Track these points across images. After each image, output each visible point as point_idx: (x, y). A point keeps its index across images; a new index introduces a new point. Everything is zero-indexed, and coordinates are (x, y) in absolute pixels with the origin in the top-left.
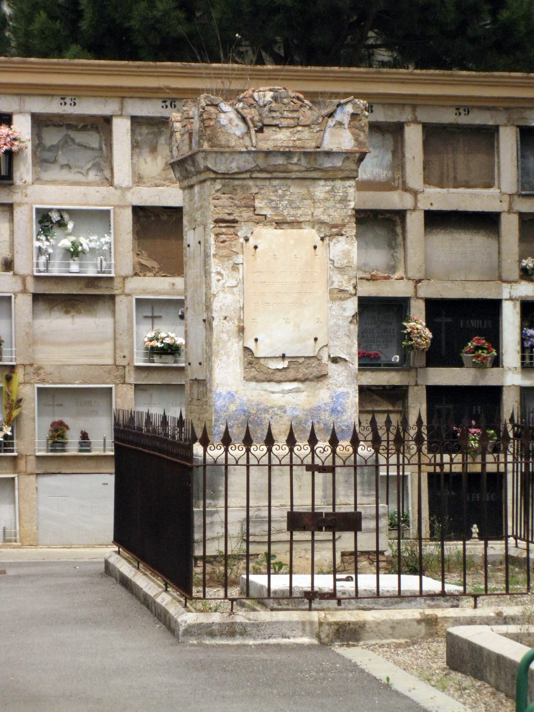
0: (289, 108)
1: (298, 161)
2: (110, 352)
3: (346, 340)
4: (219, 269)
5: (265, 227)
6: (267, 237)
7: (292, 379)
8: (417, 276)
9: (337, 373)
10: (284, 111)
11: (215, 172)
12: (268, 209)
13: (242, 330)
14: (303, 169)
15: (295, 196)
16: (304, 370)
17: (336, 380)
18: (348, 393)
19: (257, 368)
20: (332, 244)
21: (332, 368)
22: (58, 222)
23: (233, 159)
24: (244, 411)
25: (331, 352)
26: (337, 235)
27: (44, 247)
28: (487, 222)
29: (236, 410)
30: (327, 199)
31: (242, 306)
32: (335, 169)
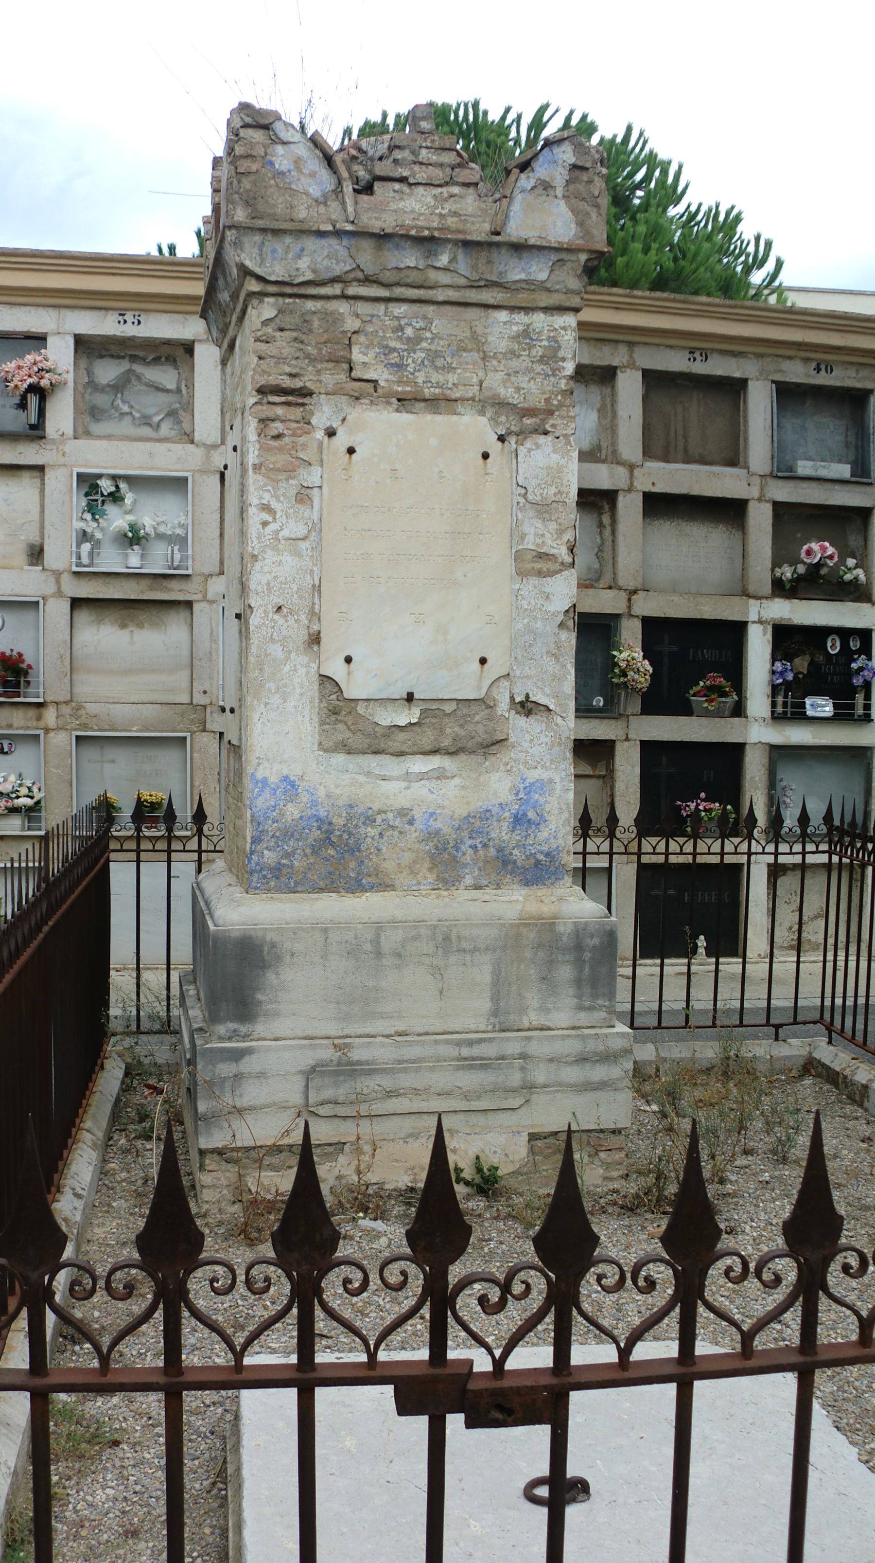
0: (433, 141)
1: (450, 262)
2: (185, 685)
3: (551, 665)
4: (267, 498)
5: (374, 407)
6: (377, 429)
7: (428, 748)
8: (632, 586)
9: (528, 737)
10: (421, 147)
11: (260, 279)
12: (380, 368)
13: (315, 639)
14: (463, 281)
15: (441, 343)
16: (456, 729)
17: (527, 752)
18: (551, 781)
19: (349, 723)
20: (522, 451)
21: (521, 728)
22: (111, 494)
23: (302, 250)
24: (319, 820)
25: (516, 690)
26: (535, 431)
27: (89, 530)
28: (730, 511)
29: (301, 818)
30: (513, 354)
31: (317, 582)
32: (531, 286)
